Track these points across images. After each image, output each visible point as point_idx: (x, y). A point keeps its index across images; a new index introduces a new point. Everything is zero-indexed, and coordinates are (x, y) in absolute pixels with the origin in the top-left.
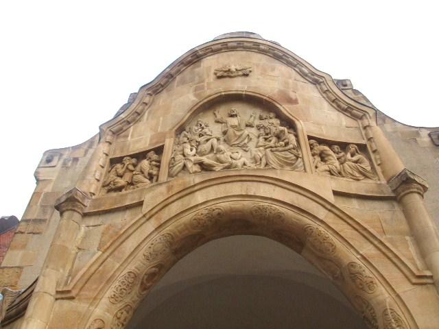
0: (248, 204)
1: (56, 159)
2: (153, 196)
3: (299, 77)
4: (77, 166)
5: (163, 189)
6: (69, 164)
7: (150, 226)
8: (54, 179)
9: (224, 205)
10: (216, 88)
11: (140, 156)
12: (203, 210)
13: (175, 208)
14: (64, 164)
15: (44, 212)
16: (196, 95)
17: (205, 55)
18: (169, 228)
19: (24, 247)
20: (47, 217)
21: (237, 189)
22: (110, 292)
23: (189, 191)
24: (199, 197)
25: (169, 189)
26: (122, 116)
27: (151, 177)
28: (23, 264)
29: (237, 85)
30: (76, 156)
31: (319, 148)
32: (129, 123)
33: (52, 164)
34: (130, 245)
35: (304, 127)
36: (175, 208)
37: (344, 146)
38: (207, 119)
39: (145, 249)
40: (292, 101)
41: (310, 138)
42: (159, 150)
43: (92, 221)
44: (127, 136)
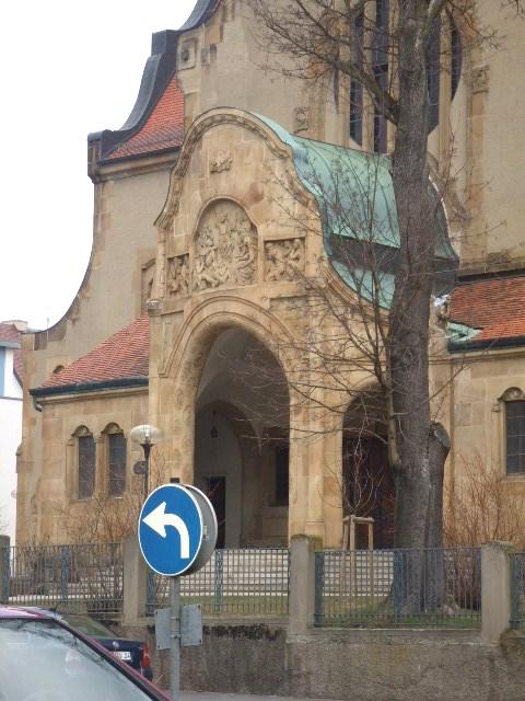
1: (192, 50)
3: (270, 155)
5: (189, 302)
7: (189, 330)
9: (215, 320)
14: (204, 61)
17: (203, 131)
18: (196, 334)
22: (181, 373)
30: (213, 42)
31: (277, 252)
32: (171, 216)
35: (264, 232)
37: (292, 240)
38: (211, 222)
39: (189, 349)
40: (257, 197)
41: (266, 242)
43: (167, 320)
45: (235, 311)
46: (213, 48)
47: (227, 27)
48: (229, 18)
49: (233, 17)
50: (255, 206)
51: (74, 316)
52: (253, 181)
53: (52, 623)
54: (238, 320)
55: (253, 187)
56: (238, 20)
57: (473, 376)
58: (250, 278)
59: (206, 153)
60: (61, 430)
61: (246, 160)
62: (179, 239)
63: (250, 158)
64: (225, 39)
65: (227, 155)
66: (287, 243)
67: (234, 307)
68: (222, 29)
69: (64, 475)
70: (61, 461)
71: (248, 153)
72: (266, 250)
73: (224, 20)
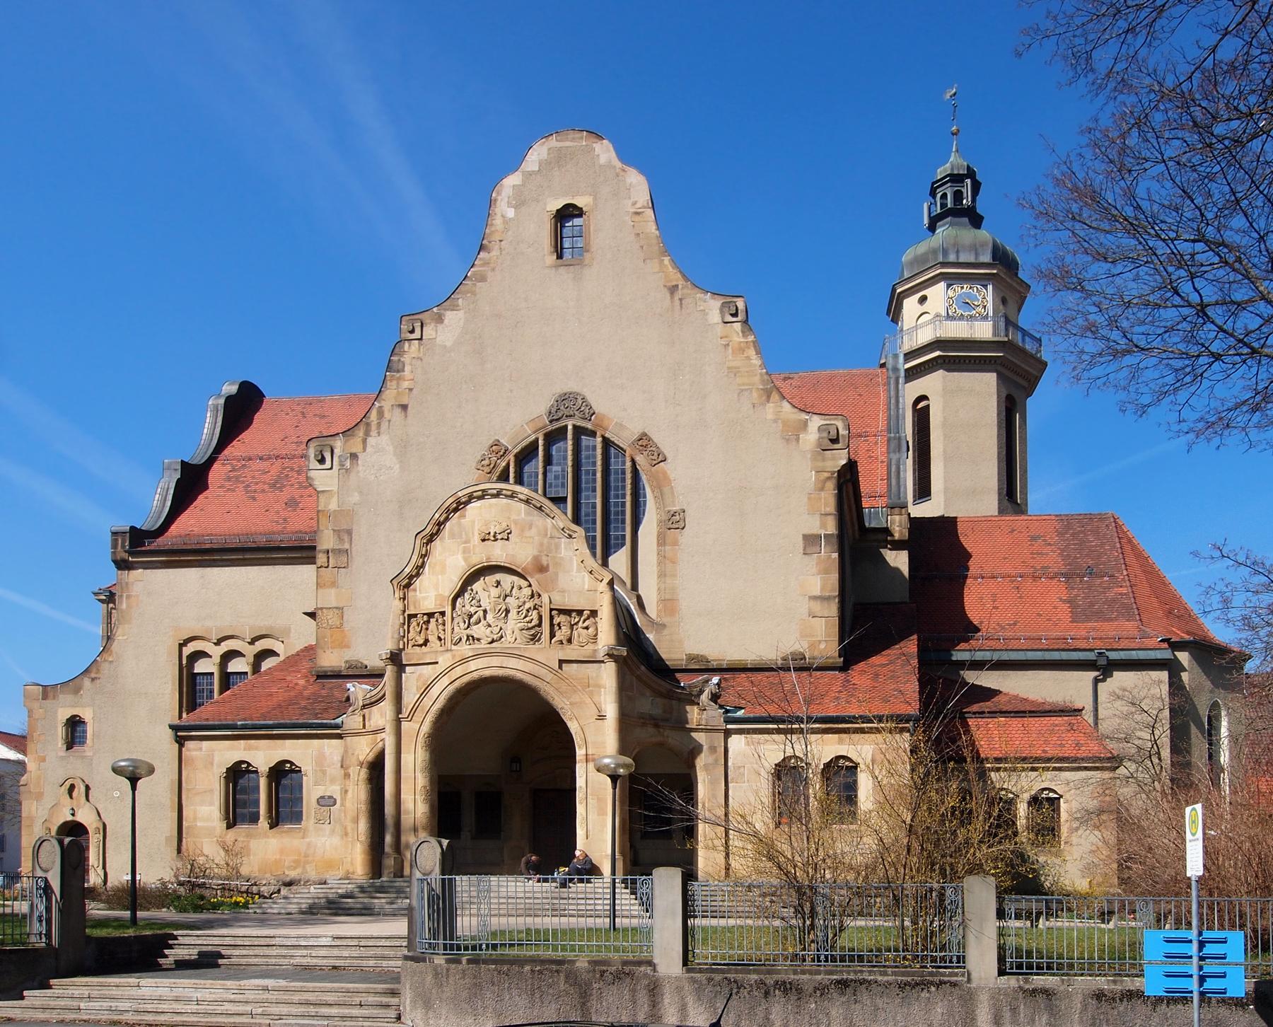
0: (500, 672)
2: (445, 661)
4: (360, 468)
5: (449, 655)
6: (348, 464)
8: (335, 488)
9: (487, 673)
10: (480, 556)
11: (431, 615)
12: (475, 675)
13: (459, 671)
15: (341, 540)
16: (465, 559)
19: (334, 584)
20: (347, 546)
21: (495, 661)
23: (464, 660)
24: (473, 665)
25: (454, 656)
26: (407, 570)
27: (440, 639)
28: (341, 605)
29: (498, 553)
30: (354, 451)
33: (328, 464)
34: (435, 691)
36: (459, 671)
37: (580, 613)
38: (478, 586)
40: (542, 569)
42: (443, 614)
44: (415, 590)
45: (514, 668)
46: (354, 456)
47: (371, 441)
48: (374, 433)
49: (379, 433)
50: (538, 576)
51: (93, 675)
52: (536, 553)
53: (923, 985)
54: (519, 675)
55: (536, 559)
56: (384, 439)
57: (748, 744)
58: (535, 638)
59: (473, 522)
60: (212, 764)
61: (527, 534)
62: (425, 598)
63: (534, 531)
64: (369, 449)
65: (504, 526)
66: (574, 614)
67: (513, 663)
68: (364, 441)
69: (217, 803)
70: (211, 791)
71: (530, 528)
72: (552, 618)
73: (367, 434)
